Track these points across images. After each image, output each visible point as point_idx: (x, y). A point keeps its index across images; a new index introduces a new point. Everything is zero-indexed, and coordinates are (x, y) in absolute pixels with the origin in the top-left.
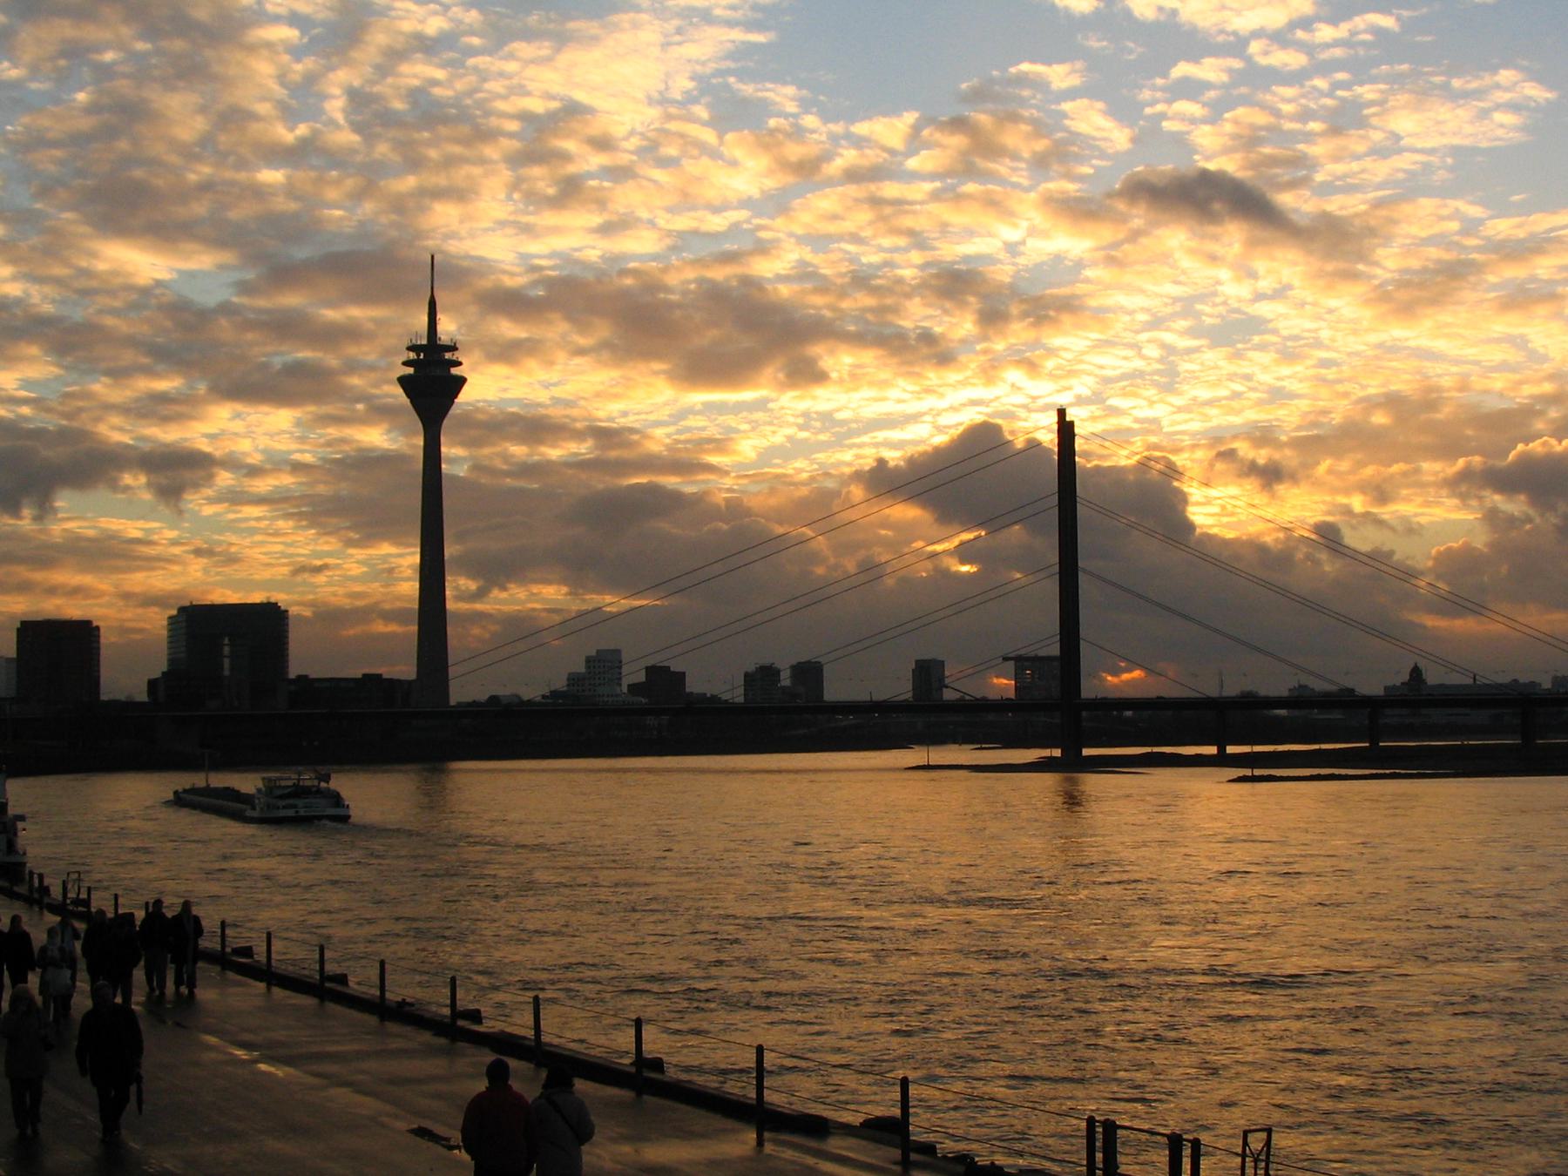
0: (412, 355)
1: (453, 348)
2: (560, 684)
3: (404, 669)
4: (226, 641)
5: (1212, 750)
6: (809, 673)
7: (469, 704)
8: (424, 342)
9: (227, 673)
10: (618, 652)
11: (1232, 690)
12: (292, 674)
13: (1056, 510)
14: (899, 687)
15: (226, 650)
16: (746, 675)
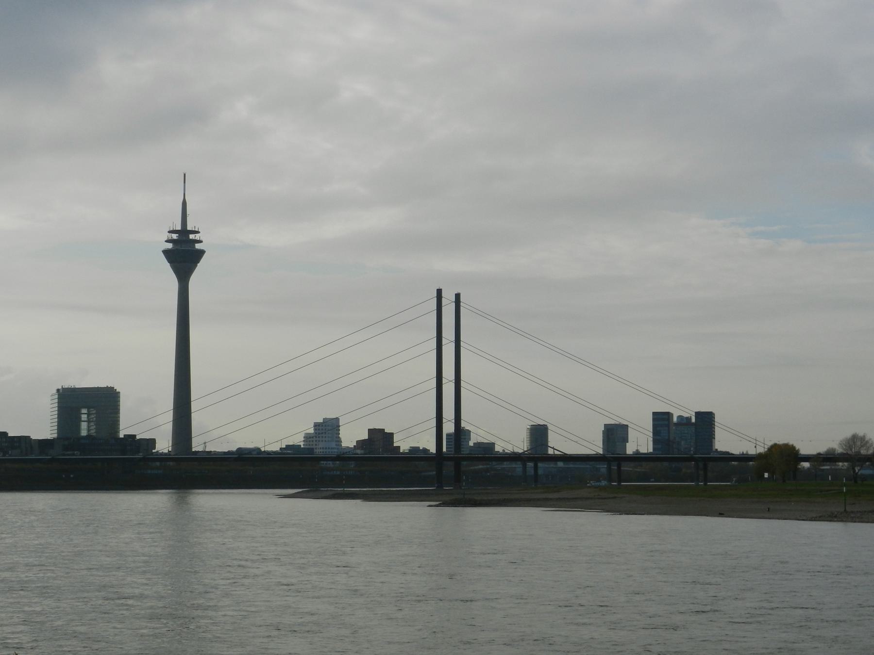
2: (298, 440)
7: (225, 453)
9: (84, 433)
10: (337, 419)
13: (192, 411)
15: (84, 417)
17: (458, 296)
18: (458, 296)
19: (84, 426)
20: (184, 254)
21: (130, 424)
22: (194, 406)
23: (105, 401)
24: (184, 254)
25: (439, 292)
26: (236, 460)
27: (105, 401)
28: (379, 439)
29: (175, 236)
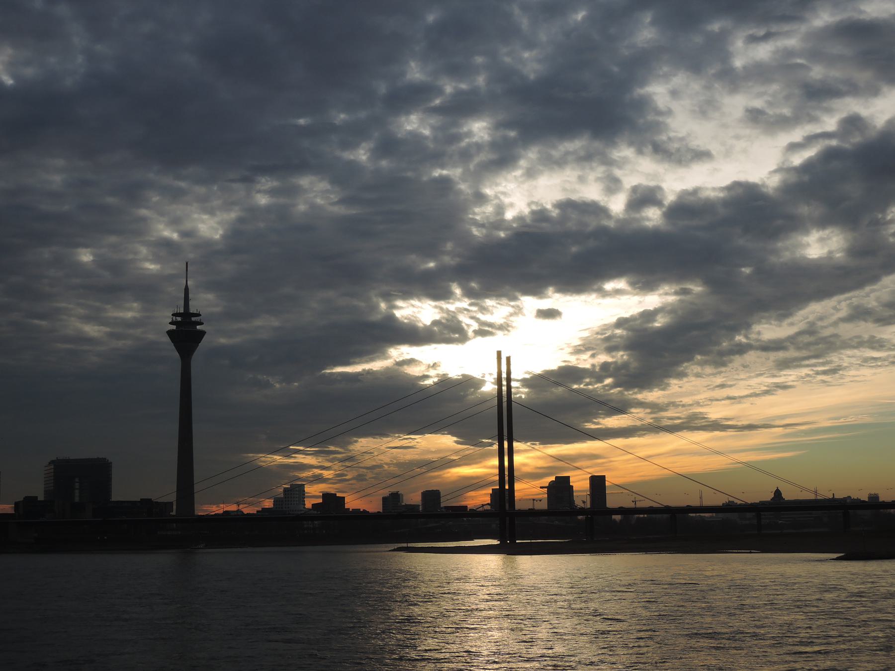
3: (163, 489)
4: (77, 480)
5: (495, 542)
7: (752, 504)
8: (182, 311)
15: (77, 485)
17: (508, 359)
18: (508, 359)
19: (77, 492)
21: (124, 489)
23: (98, 472)
25: (499, 354)
27: (98, 472)
28: (331, 501)
29: (179, 319)
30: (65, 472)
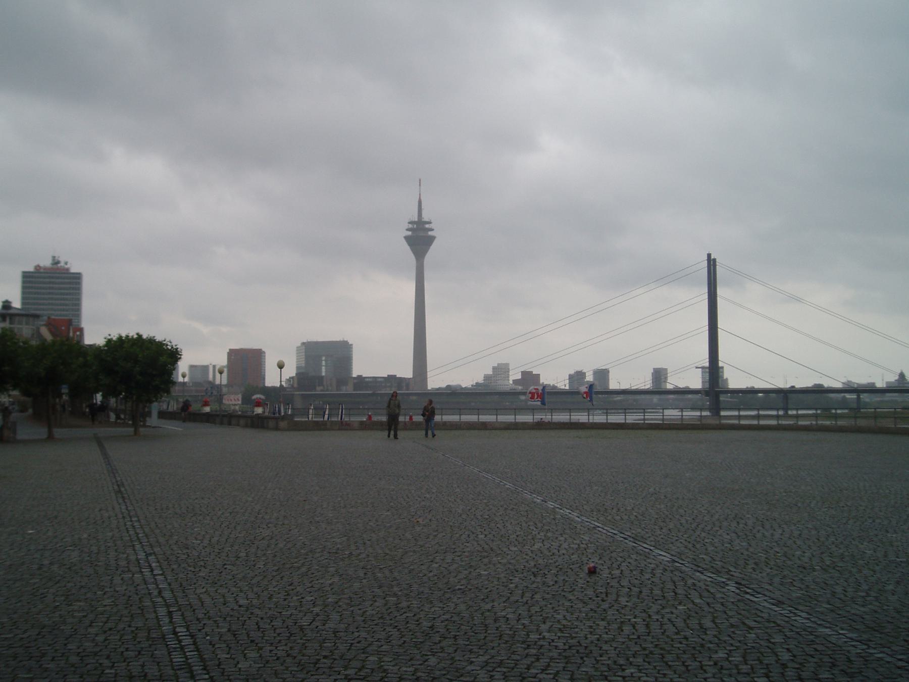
0: (410, 226)
1: (430, 223)
3: (406, 371)
6: (602, 374)
7: (438, 389)
10: (507, 365)
11: (804, 382)
12: (354, 375)
14: (644, 382)
16: (570, 375)
20: (420, 239)
22: (430, 367)
24: (420, 239)
25: (712, 263)
26: (448, 394)
30: (312, 352)
